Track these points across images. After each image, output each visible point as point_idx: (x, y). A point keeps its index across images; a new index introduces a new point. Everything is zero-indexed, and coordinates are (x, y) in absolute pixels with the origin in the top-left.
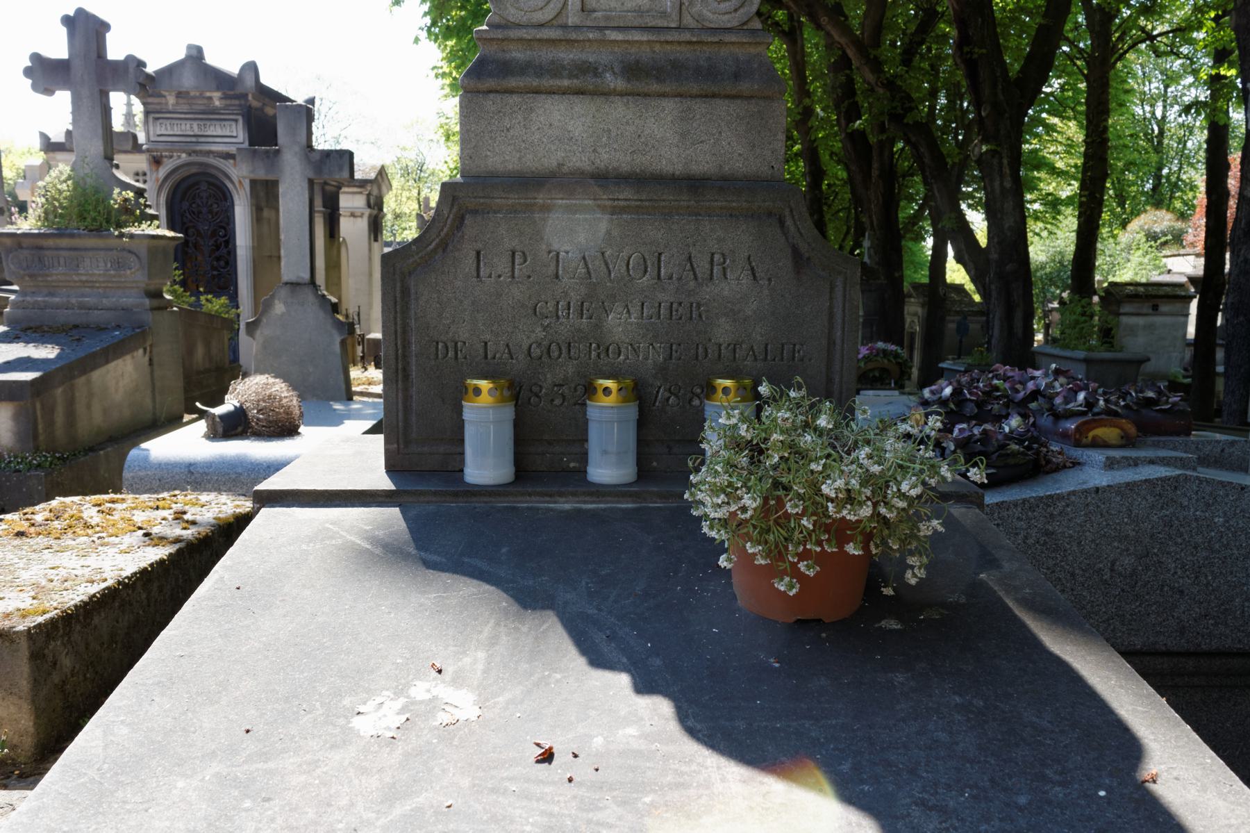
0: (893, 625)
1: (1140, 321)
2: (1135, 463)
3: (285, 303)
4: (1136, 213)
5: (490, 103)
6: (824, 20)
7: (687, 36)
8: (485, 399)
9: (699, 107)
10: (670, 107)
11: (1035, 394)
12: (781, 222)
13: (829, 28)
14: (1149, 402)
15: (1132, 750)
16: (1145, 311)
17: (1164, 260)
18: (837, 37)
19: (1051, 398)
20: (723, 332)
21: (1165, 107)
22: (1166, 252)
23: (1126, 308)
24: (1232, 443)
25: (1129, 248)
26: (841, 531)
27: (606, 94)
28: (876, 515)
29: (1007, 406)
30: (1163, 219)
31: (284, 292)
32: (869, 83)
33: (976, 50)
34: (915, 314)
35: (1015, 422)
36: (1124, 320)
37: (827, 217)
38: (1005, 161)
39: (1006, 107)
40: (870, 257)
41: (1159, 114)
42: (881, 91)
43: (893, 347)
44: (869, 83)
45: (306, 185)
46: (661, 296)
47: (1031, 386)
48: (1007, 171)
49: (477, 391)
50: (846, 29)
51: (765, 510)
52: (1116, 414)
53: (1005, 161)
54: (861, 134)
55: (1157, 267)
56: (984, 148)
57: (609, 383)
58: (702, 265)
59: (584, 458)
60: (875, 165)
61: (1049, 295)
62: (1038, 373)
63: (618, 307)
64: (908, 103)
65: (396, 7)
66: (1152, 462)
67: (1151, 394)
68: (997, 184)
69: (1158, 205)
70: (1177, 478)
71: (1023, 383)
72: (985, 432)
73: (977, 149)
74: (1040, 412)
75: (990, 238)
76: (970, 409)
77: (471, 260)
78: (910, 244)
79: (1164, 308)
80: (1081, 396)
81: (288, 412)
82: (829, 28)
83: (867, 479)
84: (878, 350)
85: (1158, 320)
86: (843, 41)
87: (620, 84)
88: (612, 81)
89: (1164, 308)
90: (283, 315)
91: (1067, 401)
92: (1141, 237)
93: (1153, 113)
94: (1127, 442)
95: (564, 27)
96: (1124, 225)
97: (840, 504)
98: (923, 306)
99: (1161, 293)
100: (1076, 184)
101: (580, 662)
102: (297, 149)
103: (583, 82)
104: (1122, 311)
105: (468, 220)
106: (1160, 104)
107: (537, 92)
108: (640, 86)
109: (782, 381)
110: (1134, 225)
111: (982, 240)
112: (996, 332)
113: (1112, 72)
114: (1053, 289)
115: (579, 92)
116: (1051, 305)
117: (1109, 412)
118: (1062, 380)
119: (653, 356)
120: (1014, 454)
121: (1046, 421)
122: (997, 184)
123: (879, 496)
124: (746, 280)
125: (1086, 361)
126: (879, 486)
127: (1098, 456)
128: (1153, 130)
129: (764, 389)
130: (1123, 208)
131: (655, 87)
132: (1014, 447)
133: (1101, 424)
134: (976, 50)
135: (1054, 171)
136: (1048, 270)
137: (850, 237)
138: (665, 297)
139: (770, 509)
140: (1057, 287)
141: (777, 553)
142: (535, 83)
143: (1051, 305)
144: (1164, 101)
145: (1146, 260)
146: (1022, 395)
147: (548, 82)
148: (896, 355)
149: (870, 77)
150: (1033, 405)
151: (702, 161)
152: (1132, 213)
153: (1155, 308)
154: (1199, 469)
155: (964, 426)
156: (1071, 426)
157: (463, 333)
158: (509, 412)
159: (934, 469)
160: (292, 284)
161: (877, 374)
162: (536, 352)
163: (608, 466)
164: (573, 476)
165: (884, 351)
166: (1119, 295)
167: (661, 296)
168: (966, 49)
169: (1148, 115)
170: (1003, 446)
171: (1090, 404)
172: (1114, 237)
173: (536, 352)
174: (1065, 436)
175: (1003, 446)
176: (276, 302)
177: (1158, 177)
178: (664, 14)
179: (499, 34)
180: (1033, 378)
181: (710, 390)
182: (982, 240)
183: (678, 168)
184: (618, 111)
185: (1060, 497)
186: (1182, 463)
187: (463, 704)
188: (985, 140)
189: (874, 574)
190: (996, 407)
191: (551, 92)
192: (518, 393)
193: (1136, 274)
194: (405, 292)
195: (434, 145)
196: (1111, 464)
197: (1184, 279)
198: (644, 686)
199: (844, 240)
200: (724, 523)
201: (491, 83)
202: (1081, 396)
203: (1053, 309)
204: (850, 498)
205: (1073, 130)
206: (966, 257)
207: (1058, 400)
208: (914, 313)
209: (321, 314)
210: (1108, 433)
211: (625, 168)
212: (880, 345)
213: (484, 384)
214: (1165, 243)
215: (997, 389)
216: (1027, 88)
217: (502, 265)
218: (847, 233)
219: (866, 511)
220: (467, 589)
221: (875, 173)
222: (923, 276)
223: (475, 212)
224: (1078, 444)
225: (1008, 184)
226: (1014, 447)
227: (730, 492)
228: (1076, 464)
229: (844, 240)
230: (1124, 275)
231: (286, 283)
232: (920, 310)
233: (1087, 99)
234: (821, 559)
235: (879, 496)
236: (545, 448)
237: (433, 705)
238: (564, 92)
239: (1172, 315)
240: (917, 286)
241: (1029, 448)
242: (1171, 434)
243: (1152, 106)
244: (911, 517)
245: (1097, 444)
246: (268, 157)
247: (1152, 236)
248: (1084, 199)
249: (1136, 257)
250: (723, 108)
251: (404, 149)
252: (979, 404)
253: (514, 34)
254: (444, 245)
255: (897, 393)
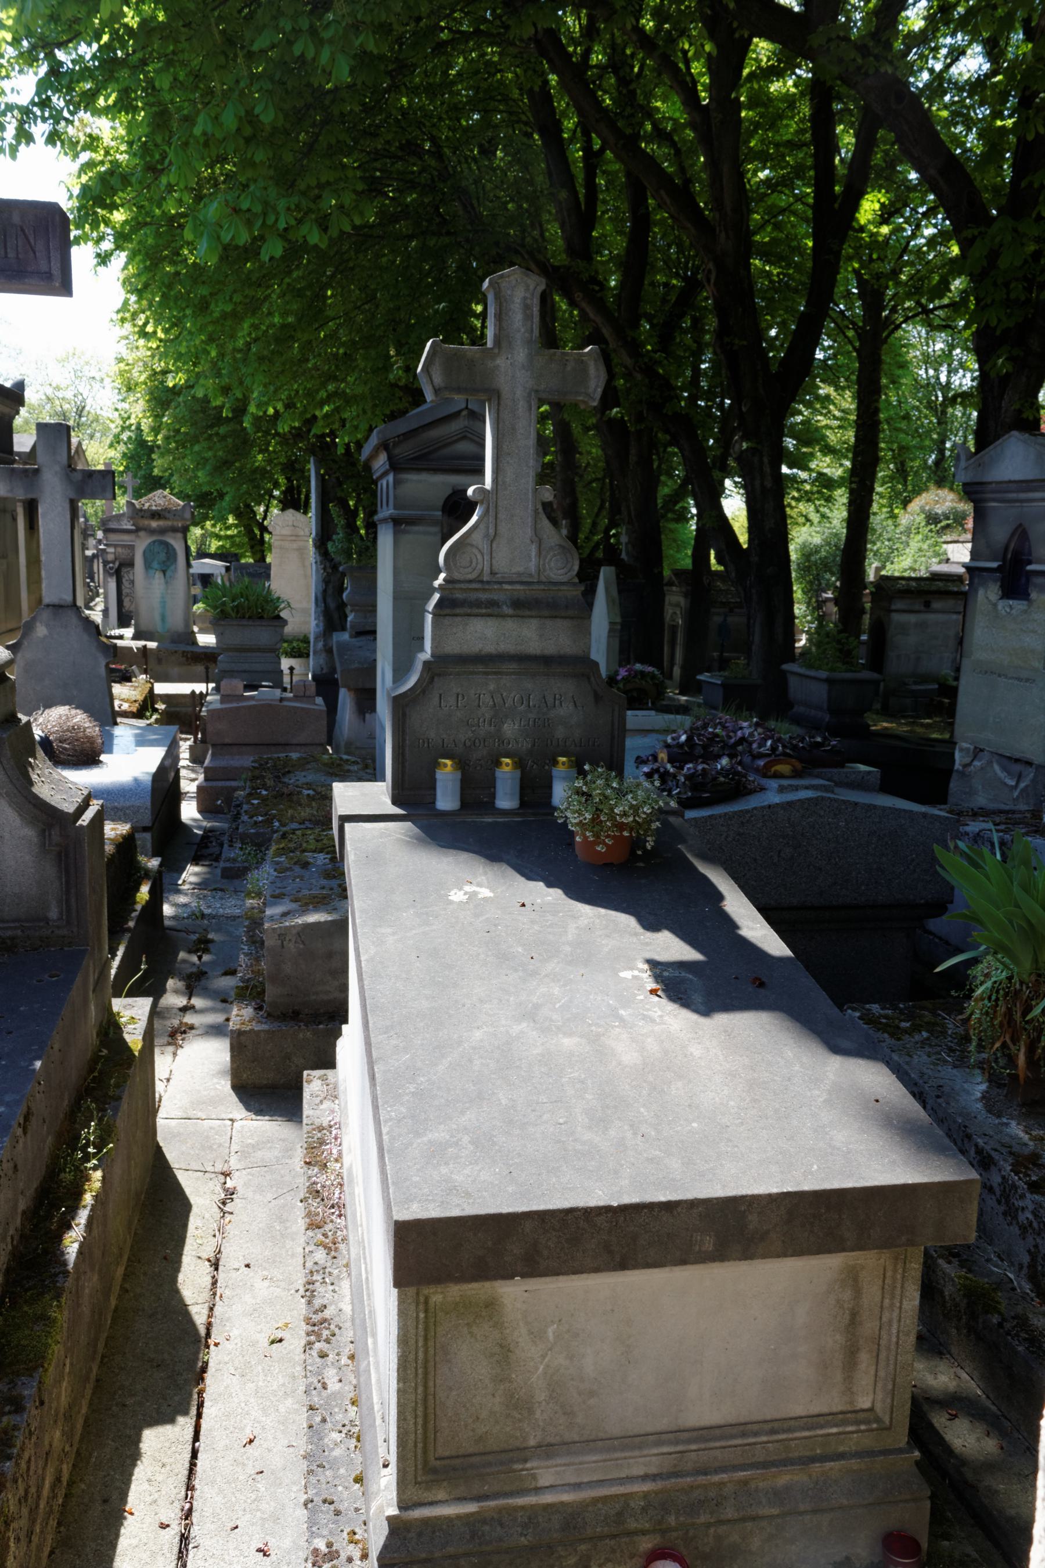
0: (642, 865)
1: (913, 618)
2: (796, 788)
3: (47, 626)
4: (918, 491)
5: (447, 621)
6: (578, 296)
7: (542, 587)
8: (449, 768)
9: (549, 623)
10: (534, 622)
11: (742, 740)
12: (589, 678)
13: (584, 305)
14: (818, 745)
15: (720, 897)
16: (917, 607)
17: (945, 546)
18: (592, 315)
19: (750, 744)
20: (560, 733)
21: (949, 372)
22: (945, 538)
23: (898, 605)
24: (869, 772)
25: (908, 532)
26: (621, 827)
27: (504, 616)
28: (635, 821)
29: (723, 748)
30: (945, 501)
31: (46, 615)
32: (626, 367)
33: (737, 341)
34: (678, 605)
35: (725, 761)
36: (896, 617)
37: (579, 488)
38: (766, 460)
39: (768, 394)
40: (627, 554)
41: (943, 378)
42: (639, 377)
43: (650, 669)
44: (626, 367)
45: (67, 506)
46: (530, 715)
47: (739, 733)
48: (767, 469)
49: (445, 765)
50: (600, 305)
51: (593, 820)
52: (789, 756)
53: (766, 460)
54: (620, 422)
55: (937, 554)
56: (745, 445)
57: (508, 760)
58: (550, 700)
59: (493, 796)
60: (633, 451)
61: (823, 582)
62: (745, 724)
63: (509, 721)
64: (666, 389)
65: (101, 269)
66: (807, 788)
67: (819, 739)
68: (757, 483)
69: (940, 483)
70: (817, 798)
71: (735, 732)
72: (704, 769)
73: (737, 446)
74: (742, 753)
75: (750, 541)
76: (699, 751)
77: (436, 700)
78: (673, 526)
79: (936, 605)
80: (769, 743)
81: (91, 740)
82: (584, 305)
83: (631, 807)
84: (636, 672)
85: (931, 617)
86: (599, 320)
87: (510, 611)
88: (507, 610)
89: (936, 605)
90: (45, 637)
91: (760, 746)
92: (921, 519)
93: (938, 378)
94: (797, 774)
95: (482, 582)
96: (906, 503)
97: (621, 816)
98: (686, 596)
99: (934, 588)
100: (848, 464)
101: (523, 879)
102: (57, 468)
103: (490, 609)
104: (893, 607)
105: (436, 679)
106: (944, 369)
107: (469, 615)
108: (519, 612)
109: (595, 764)
110: (915, 505)
111: (743, 538)
112: (757, 638)
113: (885, 347)
114: (827, 576)
115: (489, 615)
116: (824, 595)
117: (784, 754)
118: (760, 730)
119: (525, 745)
120: (722, 784)
121: (747, 759)
122: (757, 483)
123: (636, 813)
124: (571, 706)
125: (828, 681)
126: (635, 809)
127: (774, 784)
128: (937, 397)
129: (587, 767)
130: (905, 485)
131: (528, 613)
132: (722, 779)
133: (779, 762)
134: (737, 341)
135: (828, 450)
136: (823, 554)
137: (604, 513)
138: (531, 716)
139: (595, 820)
140: (833, 574)
141: (597, 836)
142: (469, 611)
143: (824, 595)
144: (949, 365)
145: (925, 547)
146: (733, 741)
147: (476, 611)
148: (653, 676)
149: (629, 362)
150: (740, 748)
151: (550, 648)
152: (913, 491)
153: (927, 604)
154: (837, 790)
155: (690, 765)
156: (761, 763)
157: (432, 734)
158: (459, 775)
159: (657, 802)
160: (54, 606)
161: (635, 694)
162: (468, 743)
163: (506, 800)
164: (488, 805)
165: (642, 673)
166: (888, 587)
167: (530, 715)
168: (726, 340)
169: (933, 381)
170: (715, 779)
171: (774, 749)
172: (893, 516)
173: (468, 743)
174: (757, 770)
175: (715, 779)
176: (38, 624)
177: (941, 451)
178: (531, 575)
179: (450, 586)
180: (741, 728)
181: (555, 763)
182: (743, 538)
183: (538, 652)
184: (510, 624)
185: (747, 811)
186: (825, 788)
187: (485, 892)
188: (745, 438)
189: (637, 843)
190: (716, 749)
191: (476, 615)
192: (462, 765)
193: (915, 561)
194: (404, 715)
195: (97, 386)
196: (782, 789)
197: (962, 570)
198: (549, 885)
199: (597, 515)
200: (577, 824)
201: (448, 611)
202: (769, 743)
203: (827, 600)
204: (625, 814)
205: (847, 401)
206: (727, 558)
207: (755, 746)
208: (675, 605)
209: (85, 637)
210: (784, 768)
211: (512, 652)
212: (638, 666)
213: (448, 762)
214: (948, 526)
215: (717, 735)
216: (795, 375)
217: (452, 701)
218: (602, 507)
219: (631, 819)
220: (464, 856)
221: (633, 459)
222: (685, 560)
223: (439, 675)
224: (765, 776)
225: (768, 484)
226: (722, 779)
227: (579, 812)
228: (762, 789)
229: (597, 515)
230: (901, 566)
231: (48, 606)
232: (682, 600)
233: (858, 377)
234: (614, 837)
235: (636, 813)
236: (476, 792)
237: (475, 893)
238: (482, 615)
239: (943, 612)
240: (679, 573)
241: (732, 779)
242: (825, 767)
243: (936, 370)
244: (648, 821)
245: (777, 776)
246: (27, 476)
247: (932, 519)
248: (854, 486)
249: (916, 542)
250: (560, 623)
251: (58, 388)
252: (705, 747)
253: (457, 586)
254: (424, 692)
255: (653, 713)
